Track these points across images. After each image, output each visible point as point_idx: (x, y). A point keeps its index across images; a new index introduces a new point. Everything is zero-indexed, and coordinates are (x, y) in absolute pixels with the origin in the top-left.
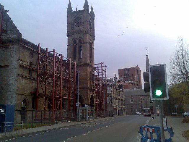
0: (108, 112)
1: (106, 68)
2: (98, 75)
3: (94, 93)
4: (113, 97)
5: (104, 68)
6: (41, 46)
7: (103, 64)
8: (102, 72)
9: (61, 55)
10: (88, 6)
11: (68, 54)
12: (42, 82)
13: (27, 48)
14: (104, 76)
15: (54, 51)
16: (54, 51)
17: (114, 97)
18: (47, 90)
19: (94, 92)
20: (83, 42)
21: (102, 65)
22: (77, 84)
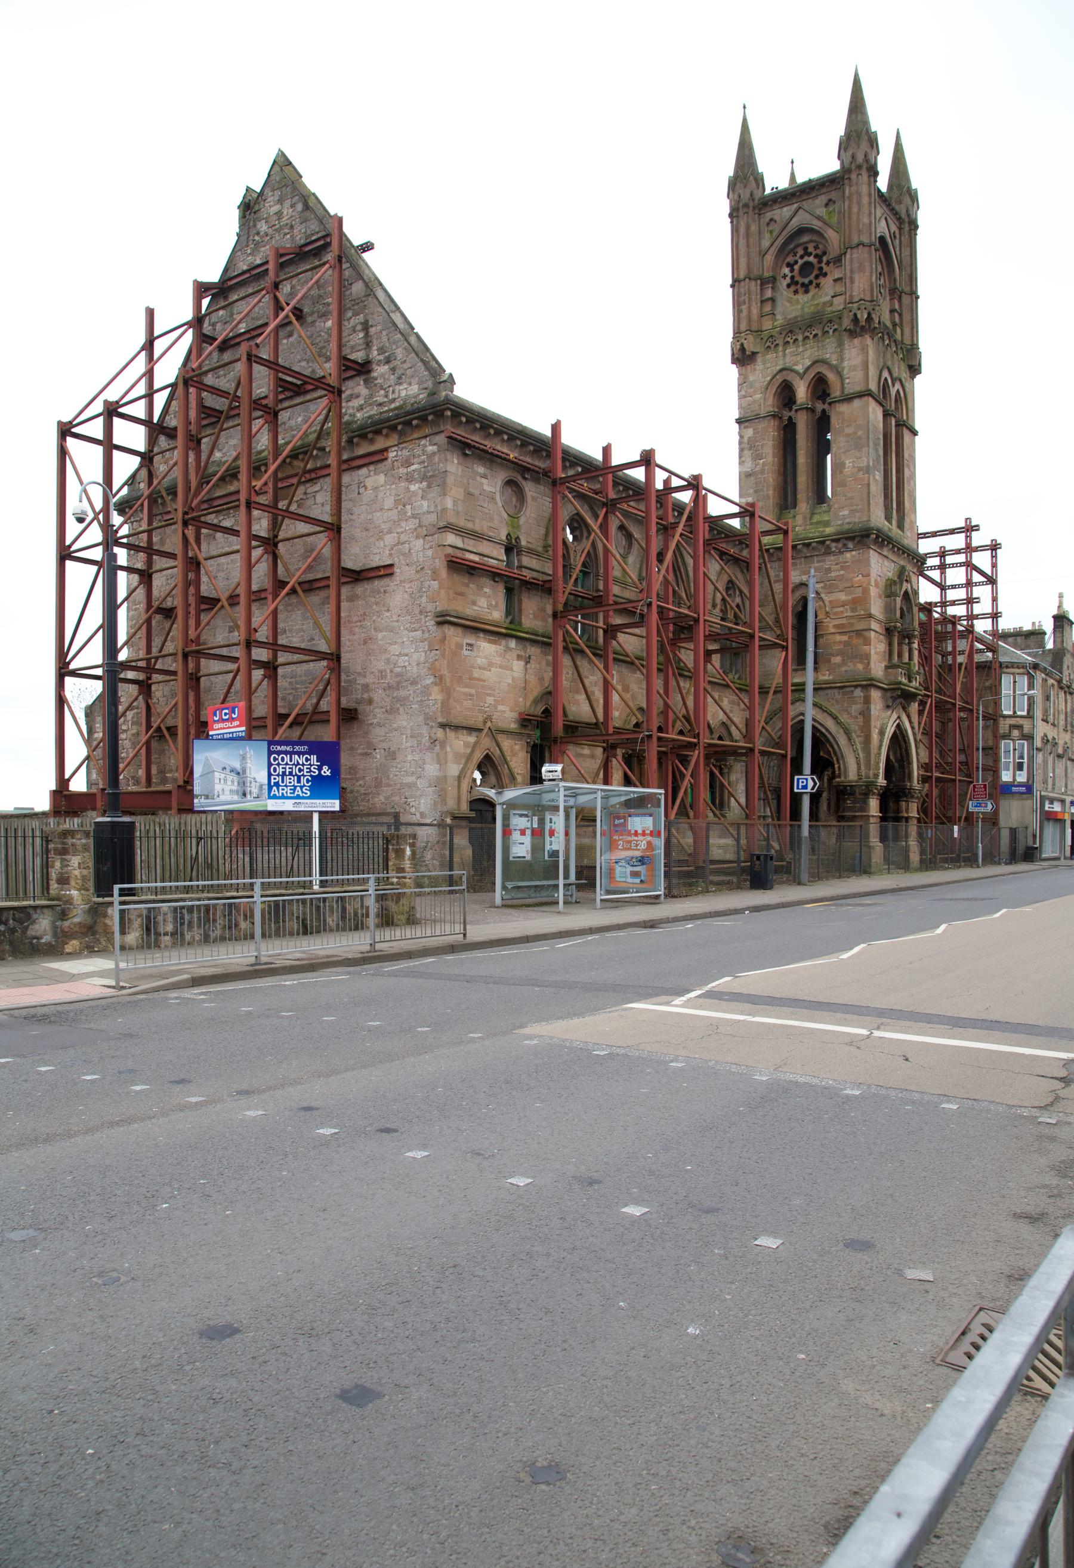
0: (1005, 834)
1: (994, 557)
2: (944, 604)
3: (915, 718)
4: (1038, 743)
5: (982, 560)
6: (569, 439)
7: (976, 528)
8: (969, 584)
9: (694, 483)
10: (873, 142)
11: (745, 477)
12: (582, 652)
13: (491, 458)
14: (983, 607)
15: (647, 459)
16: (647, 459)
17: (1046, 740)
18: (615, 698)
19: (914, 707)
20: (836, 393)
21: (968, 538)
22: (801, 660)
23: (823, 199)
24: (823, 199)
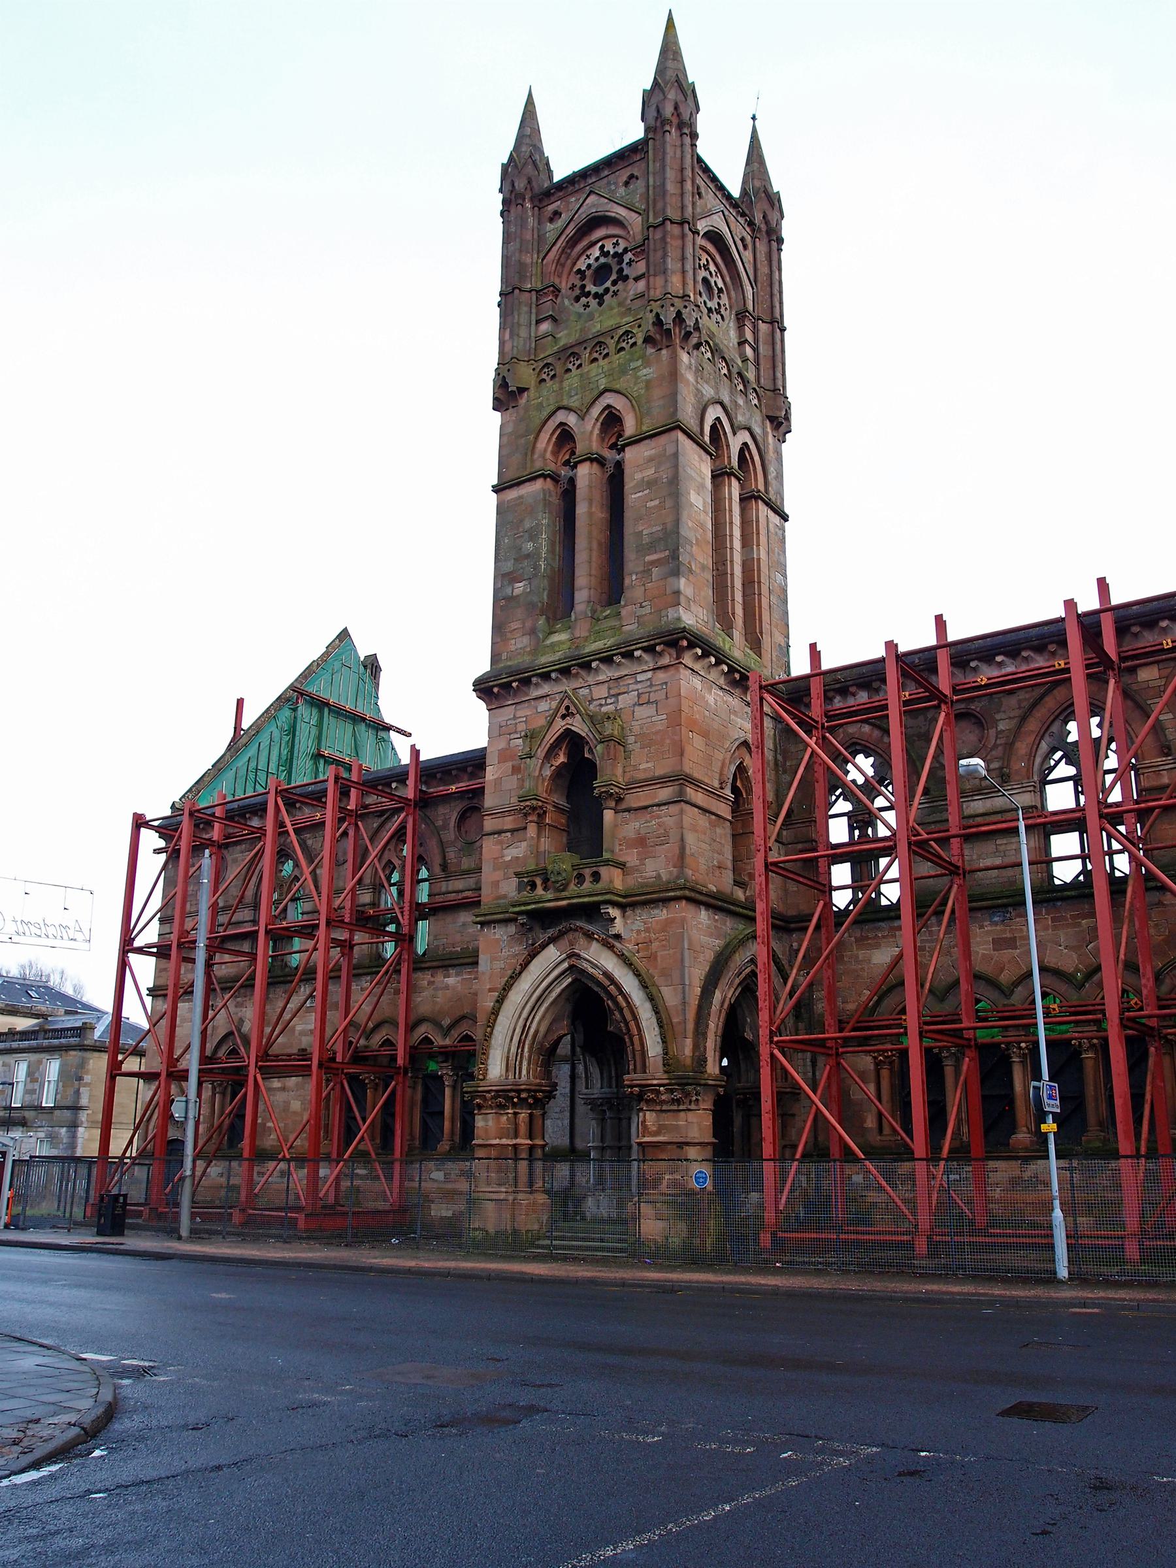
23: (624, 175)
24: (624, 175)
